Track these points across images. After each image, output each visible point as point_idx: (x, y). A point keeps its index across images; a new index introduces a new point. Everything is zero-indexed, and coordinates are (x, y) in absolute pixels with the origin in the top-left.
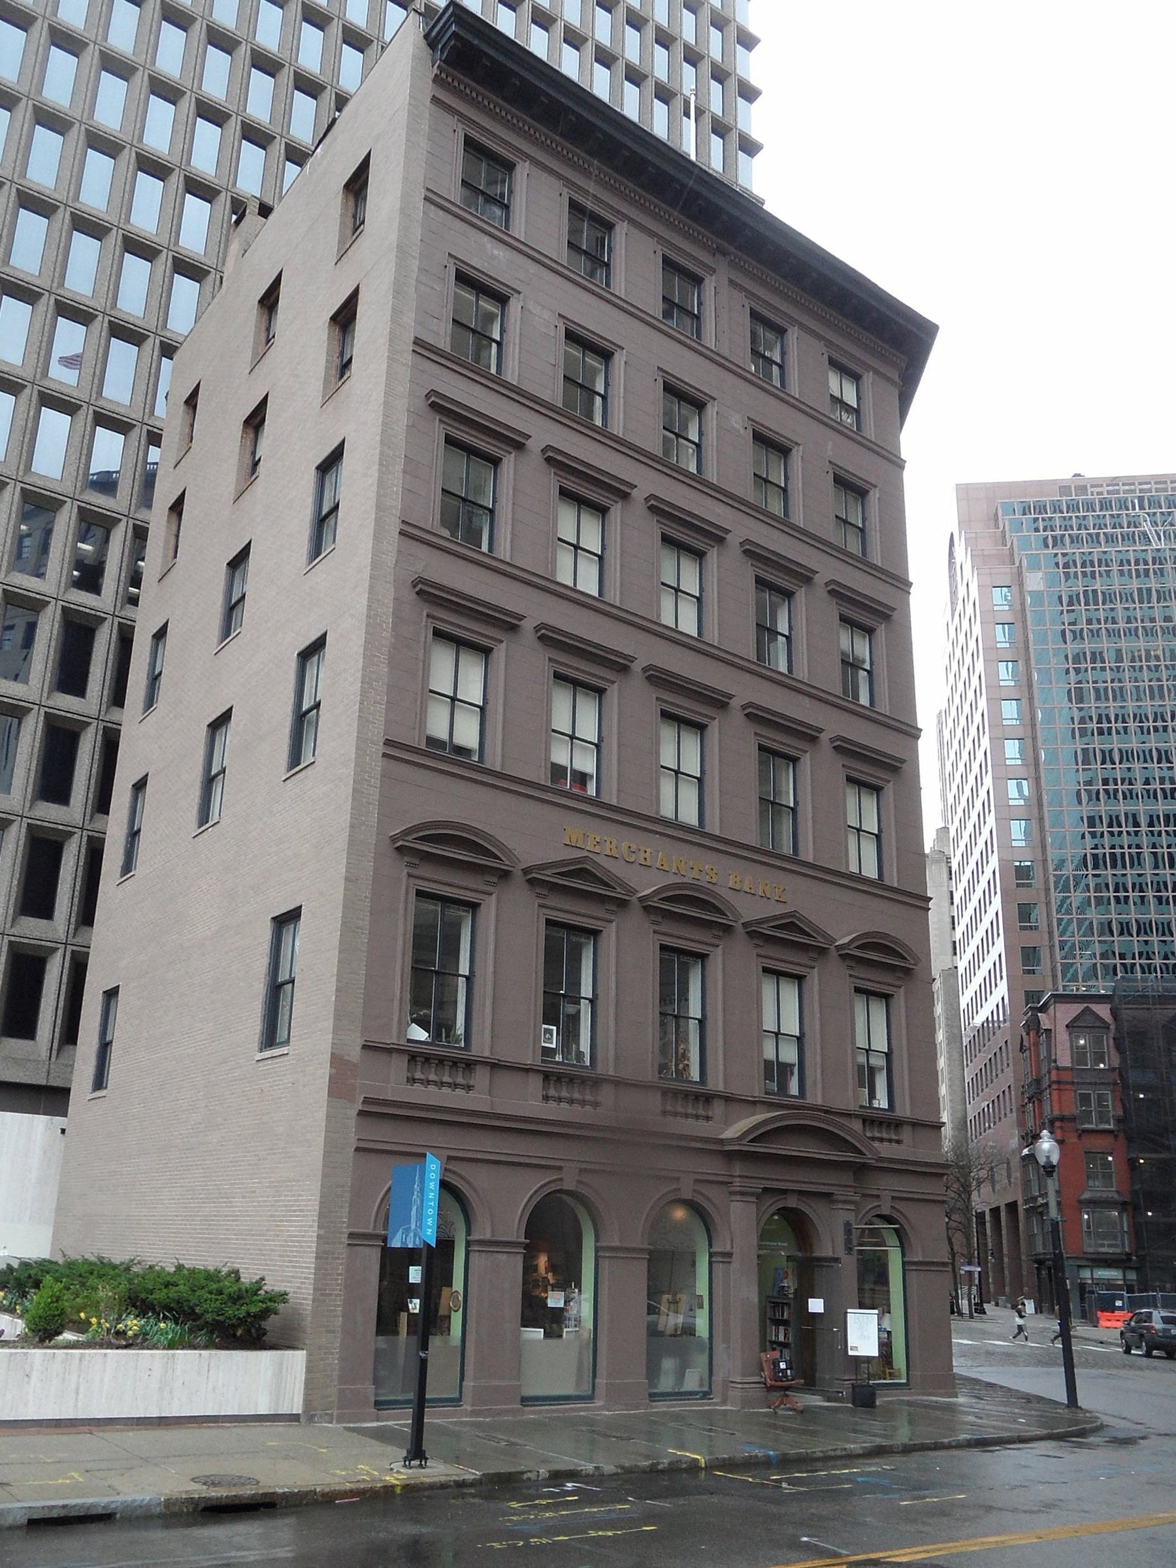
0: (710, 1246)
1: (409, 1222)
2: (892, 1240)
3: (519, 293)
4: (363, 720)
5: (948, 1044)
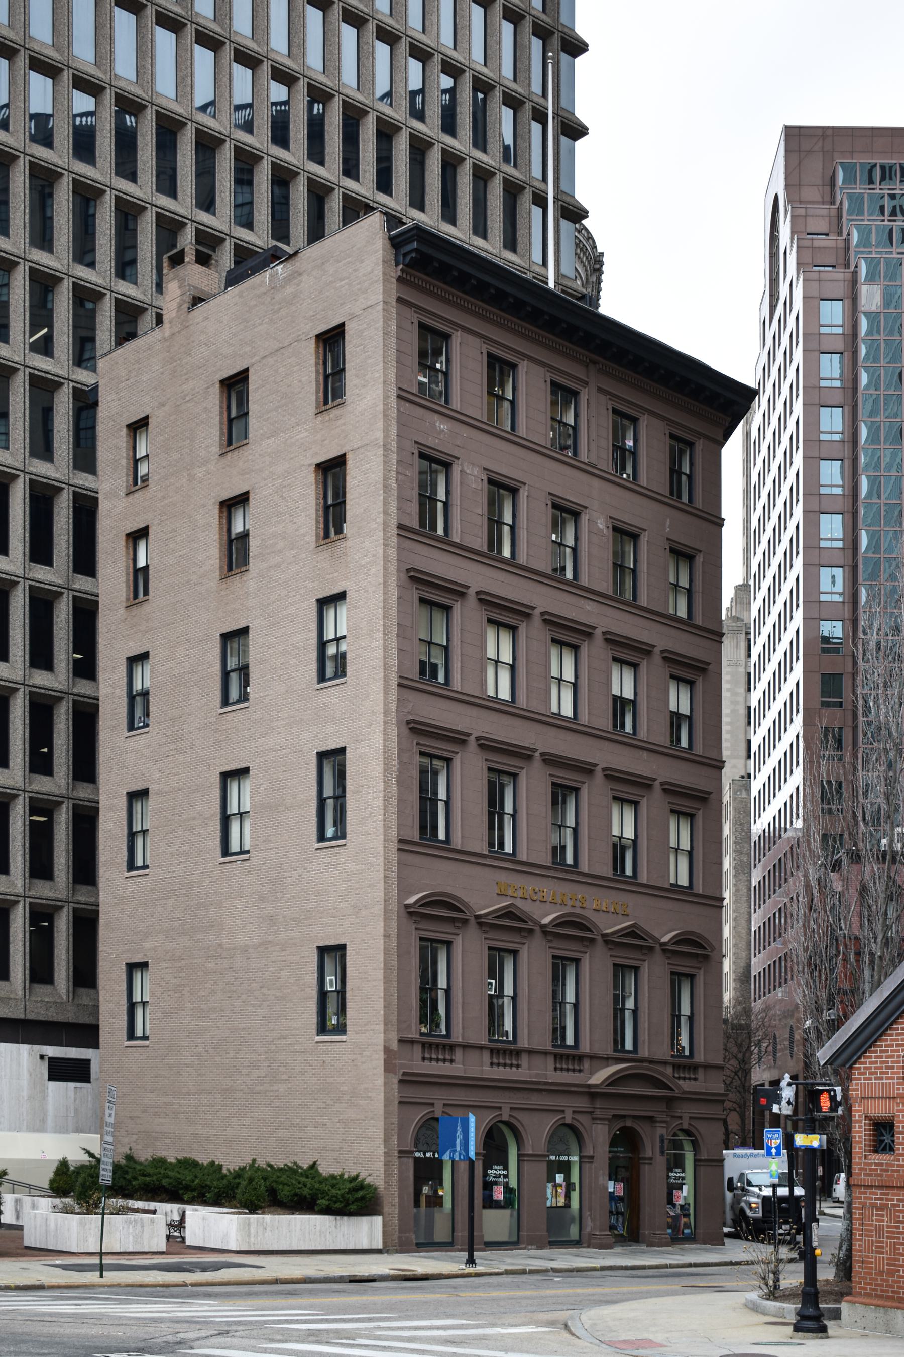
0: (580, 1152)
1: (455, 1146)
2: (688, 1147)
3: (458, 459)
4: (386, 827)
5: (735, 876)
